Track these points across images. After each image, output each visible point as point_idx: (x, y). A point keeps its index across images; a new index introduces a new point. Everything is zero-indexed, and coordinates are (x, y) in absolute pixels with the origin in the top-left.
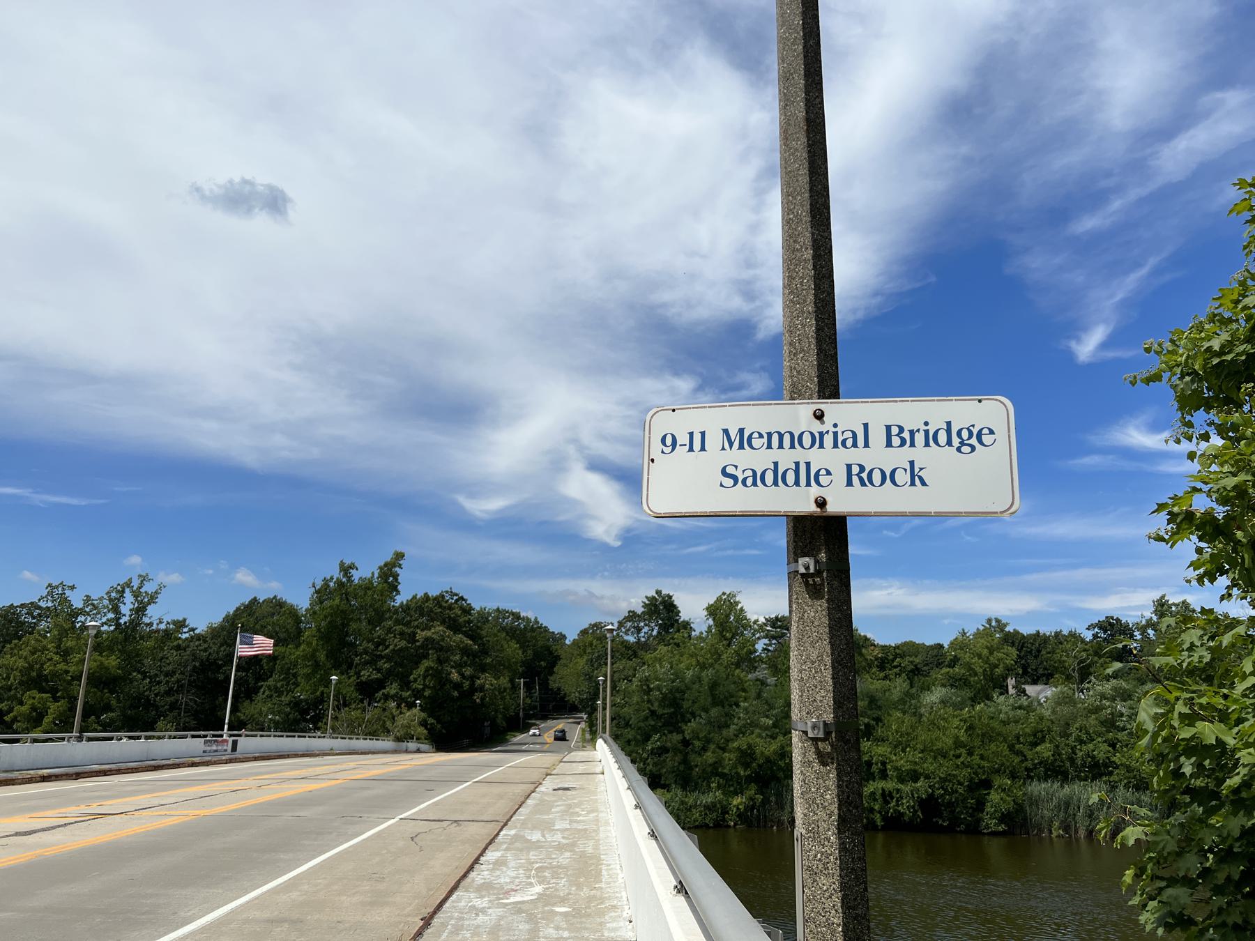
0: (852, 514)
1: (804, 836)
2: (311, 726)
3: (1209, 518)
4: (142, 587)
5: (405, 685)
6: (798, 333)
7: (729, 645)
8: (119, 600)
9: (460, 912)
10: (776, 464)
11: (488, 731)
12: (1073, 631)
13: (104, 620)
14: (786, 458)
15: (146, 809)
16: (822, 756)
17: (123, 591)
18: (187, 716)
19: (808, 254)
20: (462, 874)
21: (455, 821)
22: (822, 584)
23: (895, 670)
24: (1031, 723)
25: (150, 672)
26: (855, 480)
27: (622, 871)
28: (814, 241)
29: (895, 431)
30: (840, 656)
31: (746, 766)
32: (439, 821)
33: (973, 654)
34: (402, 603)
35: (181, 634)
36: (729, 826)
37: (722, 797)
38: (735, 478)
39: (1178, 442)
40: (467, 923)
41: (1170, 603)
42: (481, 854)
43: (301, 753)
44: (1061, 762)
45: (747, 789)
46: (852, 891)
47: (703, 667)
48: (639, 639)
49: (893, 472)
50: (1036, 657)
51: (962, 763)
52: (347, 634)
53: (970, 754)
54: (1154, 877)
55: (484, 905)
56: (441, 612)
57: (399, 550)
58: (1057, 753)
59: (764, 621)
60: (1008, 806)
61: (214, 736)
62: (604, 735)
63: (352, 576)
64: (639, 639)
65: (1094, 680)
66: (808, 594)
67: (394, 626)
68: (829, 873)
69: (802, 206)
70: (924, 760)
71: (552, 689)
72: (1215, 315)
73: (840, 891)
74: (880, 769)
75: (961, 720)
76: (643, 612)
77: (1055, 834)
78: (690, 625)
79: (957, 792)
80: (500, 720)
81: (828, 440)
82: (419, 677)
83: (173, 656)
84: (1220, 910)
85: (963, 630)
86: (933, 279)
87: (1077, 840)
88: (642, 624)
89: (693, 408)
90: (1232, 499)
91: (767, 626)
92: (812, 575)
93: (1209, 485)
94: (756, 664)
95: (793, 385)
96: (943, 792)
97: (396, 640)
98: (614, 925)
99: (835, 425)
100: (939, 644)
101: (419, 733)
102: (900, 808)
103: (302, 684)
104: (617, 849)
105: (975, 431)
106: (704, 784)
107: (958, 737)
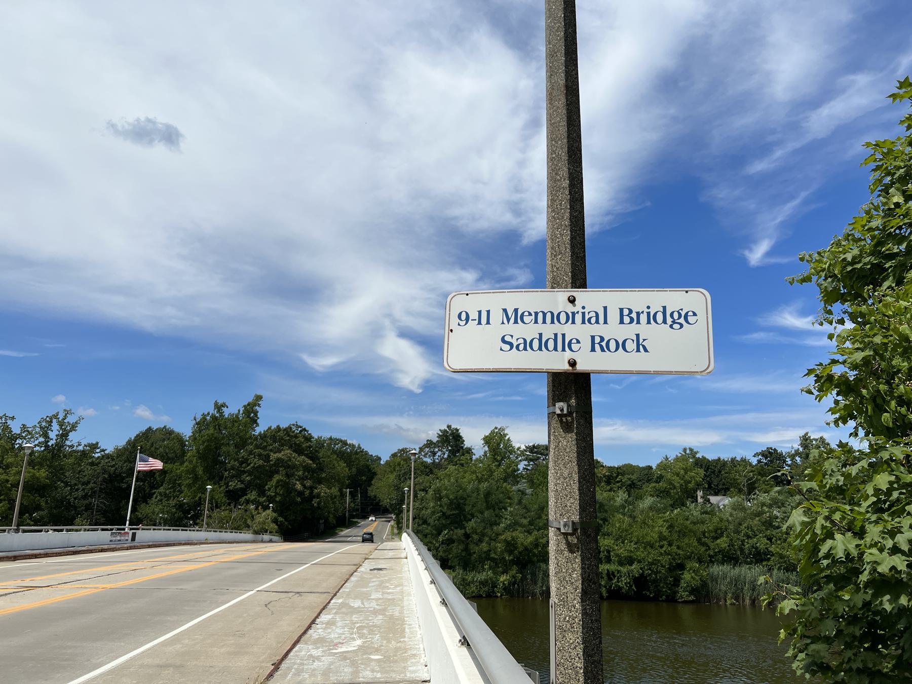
0: (595, 371)
1: (557, 604)
2: (191, 522)
3: (844, 378)
4: (66, 418)
5: (262, 493)
6: (558, 240)
7: (499, 465)
8: (48, 428)
9: (301, 660)
10: (541, 335)
11: (322, 527)
12: (744, 457)
13: (37, 442)
14: (548, 331)
15: (67, 583)
16: (570, 546)
17: (51, 422)
18: (98, 515)
19: (566, 183)
20: (303, 631)
21: (298, 593)
22: (573, 422)
23: (618, 484)
24: (714, 523)
25: (71, 482)
26: (597, 347)
27: (420, 629)
28: (570, 174)
29: (626, 312)
30: (584, 474)
31: (511, 552)
32: (286, 592)
33: (673, 473)
34: (261, 432)
35: (95, 453)
36: (497, 597)
37: (492, 575)
38: (511, 344)
39: (821, 324)
40: (306, 667)
41: (811, 438)
42: (317, 617)
43: (184, 542)
44: (734, 550)
45: (510, 569)
46: (591, 644)
47: (480, 481)
48: (434, 461)
49: (624, 342)
50: (718, 476)
51: (665, 551)
52: (219, 455)
53: (670, 545)
54: (803, 636)
55: (319, 654)
56: (289, 440)
57: (259, 393)
58: (731, 545)
59: (525, 448)
60: (696, 583)
61: (118, 529)
62: (408, 530)
63: (224, 412)
64: (434, 461)
65: (758, 493)
66: (562, 429)
67: (254, 449)
68: (574, 631)
69: (562, 148)
70: (637, 549)
71: (370, 497)
72: (849, 235)
73: (582, 644)
74: (606, 555)
75: (664, 521)
76: (438, 441)
77: (729, 602)
78: (471, 450)
79: (660, 572)
80: (332, 520)
81: (578, 318)
82: (272, 487)
83: (88, 471)
84: (850, 659)
85: (666, 456)
86: (648, 204)
87: (744, 607)
88: (437, 450)
89: (482, 293)
90: (860, 366)
91: (526, 452)
92: (565, 415)
93: (844, 357)
94: (518, 479)
95: (554, 278)
96: (650, 572)
97: (256, 460)
98: (414, 668)
99: (583, 308)
100: (649, 466)
101: (271, 528)
102: (620, 584)
103: (185, 492)
104: (417, 613)
105: (683, 314)
106: (480, 565)
107: (661, 533)
